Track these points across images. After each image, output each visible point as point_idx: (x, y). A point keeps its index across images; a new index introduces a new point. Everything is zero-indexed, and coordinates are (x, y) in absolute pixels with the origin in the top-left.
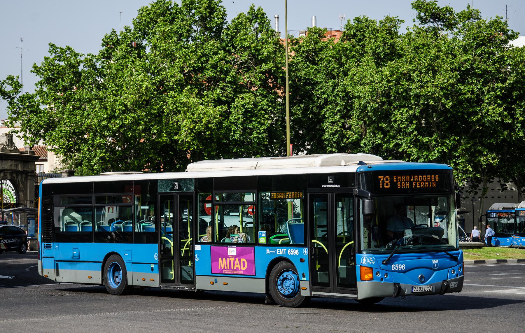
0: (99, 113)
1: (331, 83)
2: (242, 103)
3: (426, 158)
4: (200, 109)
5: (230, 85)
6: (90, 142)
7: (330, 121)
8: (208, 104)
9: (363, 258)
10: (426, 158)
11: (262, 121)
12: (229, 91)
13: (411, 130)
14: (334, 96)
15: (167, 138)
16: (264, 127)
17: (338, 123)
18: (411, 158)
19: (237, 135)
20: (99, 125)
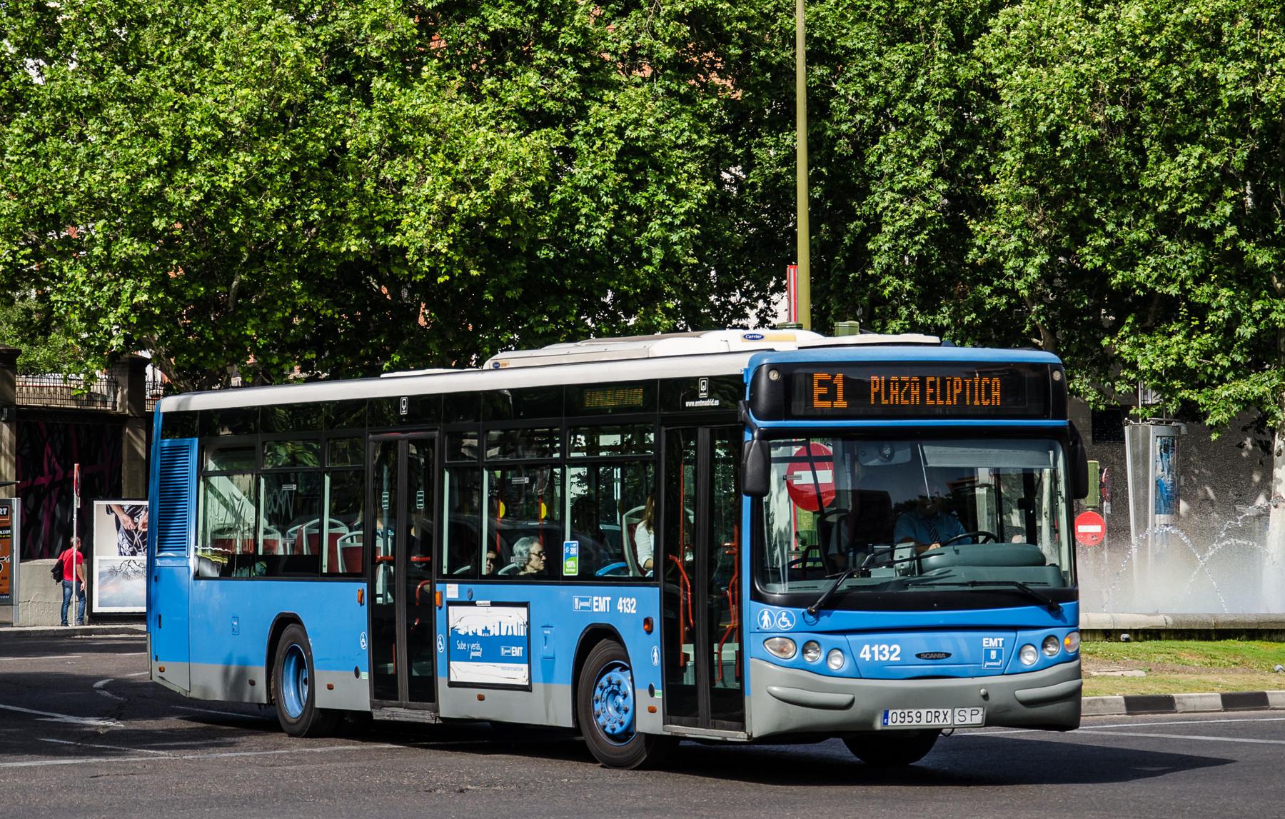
0: (132, 151)
1: (896, 56)
2: (616, 121)
3: (1261, 319)
4: (480, 140)
5: (570, 59)
6: (97, 251)
7: (898, 187)
8: (498, 124)
9: (762, 614)
10: (1261, 319)
11: (683, 186)
12: (567, 81)
13: (1217, 223)
14: (912, 101)
15: (364, 241)
16: (687, 205)
17: (927, 193)
18: (1211, 318)
19: (600, 231)
20: (133, 191)
